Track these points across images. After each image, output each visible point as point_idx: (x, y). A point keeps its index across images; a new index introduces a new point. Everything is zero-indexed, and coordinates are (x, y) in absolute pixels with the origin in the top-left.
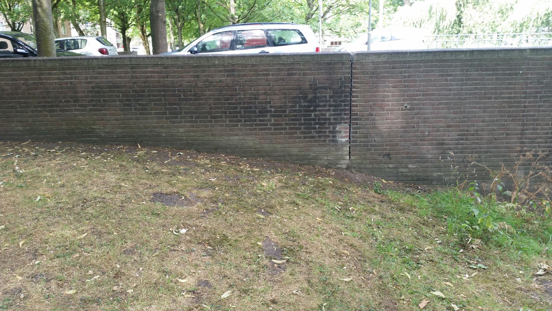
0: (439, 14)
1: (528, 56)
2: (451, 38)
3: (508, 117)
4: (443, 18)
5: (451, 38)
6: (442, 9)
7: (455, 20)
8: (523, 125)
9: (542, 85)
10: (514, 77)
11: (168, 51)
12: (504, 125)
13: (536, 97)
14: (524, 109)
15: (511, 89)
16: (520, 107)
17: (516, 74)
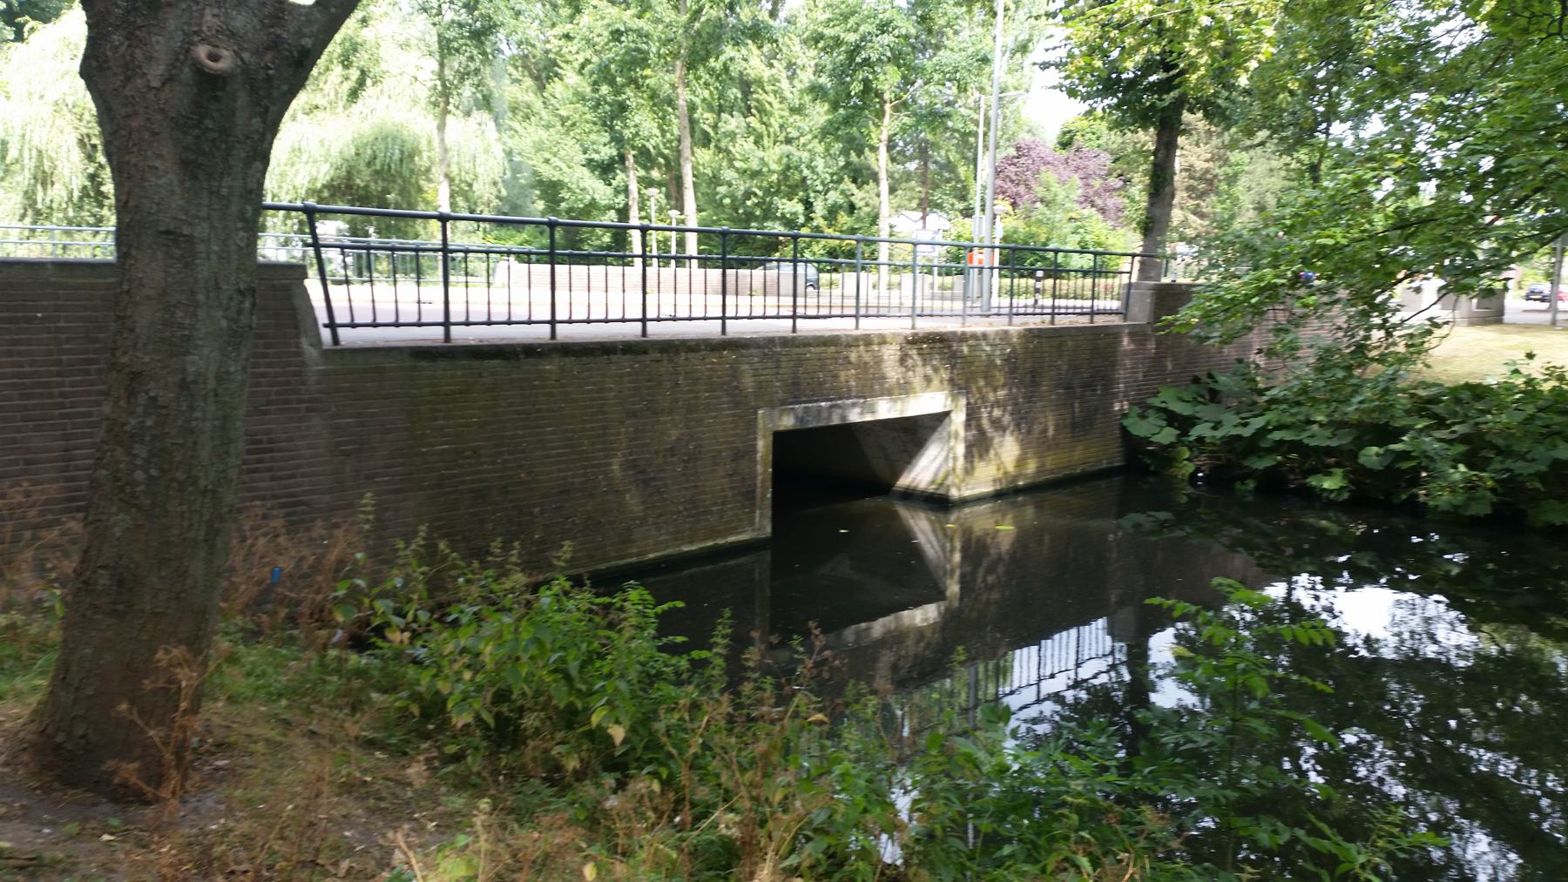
0: (30, 164)
1: (53, 279)
2: (76, 236)
3: (22, 421)
4: (44, 178)
5: (76, 236)
6: (40, 152)
7: (85, 187)
8: (67, 437)
9: (97, 346)
10: (25, 326)
11: (309, 46)
12: (15, 441)
13: (87, 373)
14: (60, 400)
15: (20, 354)
16: (51, 396)
17: (29, 320)
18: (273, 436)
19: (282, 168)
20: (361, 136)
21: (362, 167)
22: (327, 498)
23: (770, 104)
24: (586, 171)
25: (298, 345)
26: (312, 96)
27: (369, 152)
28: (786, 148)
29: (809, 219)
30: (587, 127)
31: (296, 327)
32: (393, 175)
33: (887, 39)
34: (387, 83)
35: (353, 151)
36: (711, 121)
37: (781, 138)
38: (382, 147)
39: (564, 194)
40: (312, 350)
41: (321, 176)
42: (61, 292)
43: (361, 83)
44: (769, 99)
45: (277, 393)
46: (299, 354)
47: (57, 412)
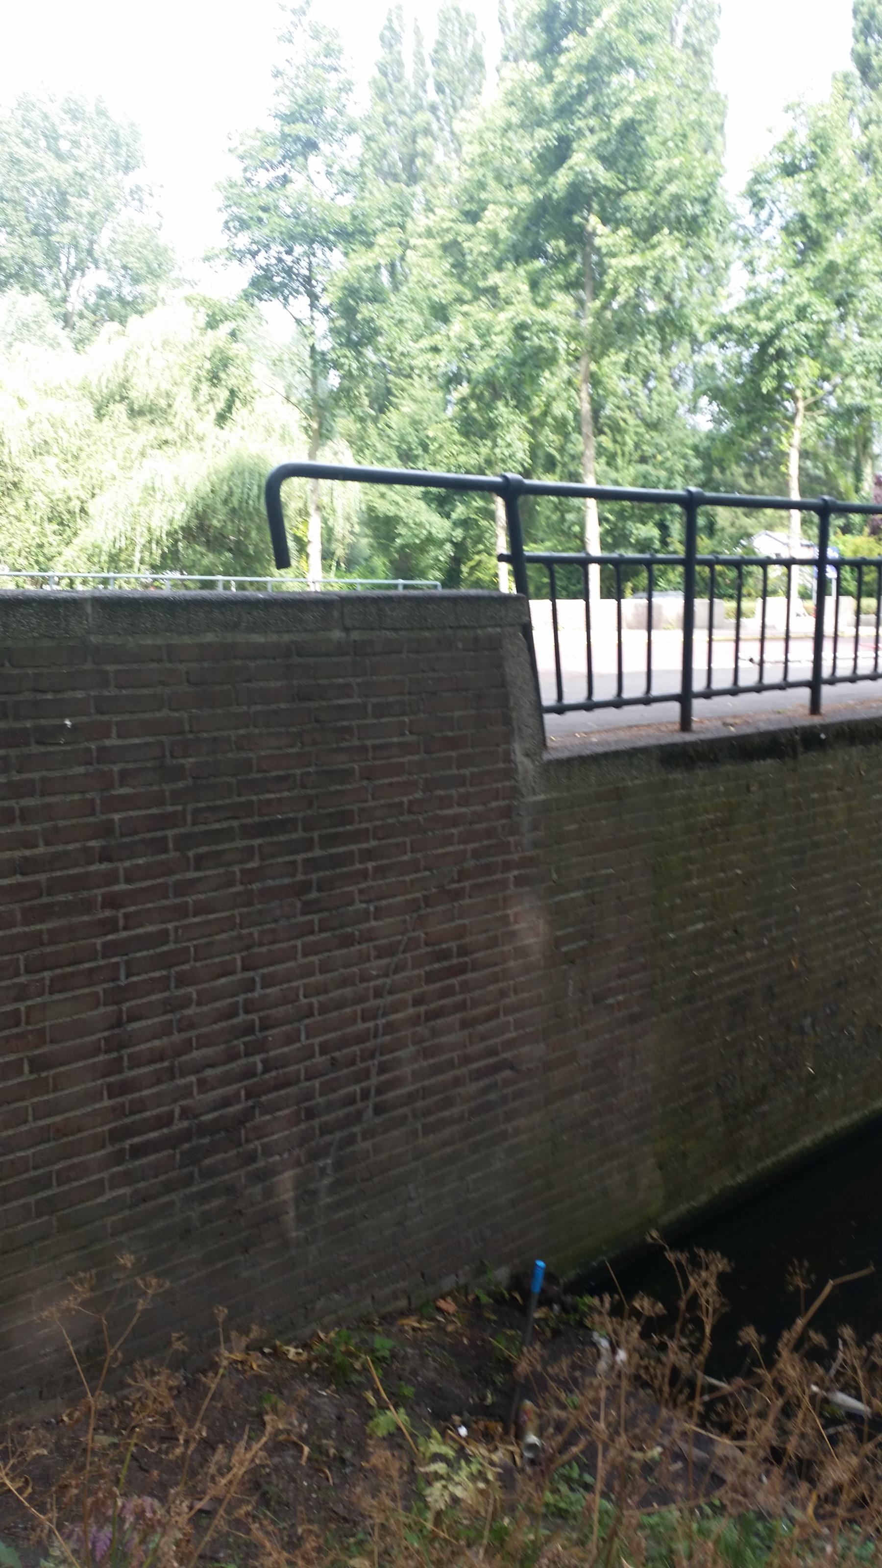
8: (116, 996)
9: (180, 785)
10: (35, 749)
13: (160, 846)
15: (26, 816)
16: (88, 906)
17: (45, 736)
18: (467, 940)
19: (136, 508)
20: (217, 472)
21: (219, 506)
22: (539, 1049)
23: (625, 421)
24: (422, 504)
25: (508, 757)
26: (160, 430)
27: (226, 488)
28: (643, 468)
29: (664, 543)
30: (455, 449)
31: (507, 720)
32: (250, 513)
33: (804, 327)
34: (258, 404)
35: (208, 489)
36: (557, 443)
37: (636, 456)
38: (239, 483)
39: (402, 530)
40: (527, 762)
41: (178, 517)
42: (111, 668)
43: (229, 407)
44: (624, 415)
45: (476, 854)
46: (509, 773)
47: (99, 942)
